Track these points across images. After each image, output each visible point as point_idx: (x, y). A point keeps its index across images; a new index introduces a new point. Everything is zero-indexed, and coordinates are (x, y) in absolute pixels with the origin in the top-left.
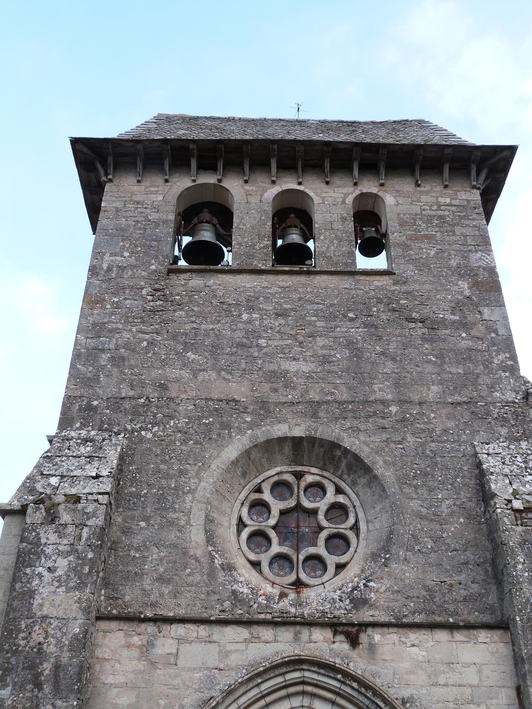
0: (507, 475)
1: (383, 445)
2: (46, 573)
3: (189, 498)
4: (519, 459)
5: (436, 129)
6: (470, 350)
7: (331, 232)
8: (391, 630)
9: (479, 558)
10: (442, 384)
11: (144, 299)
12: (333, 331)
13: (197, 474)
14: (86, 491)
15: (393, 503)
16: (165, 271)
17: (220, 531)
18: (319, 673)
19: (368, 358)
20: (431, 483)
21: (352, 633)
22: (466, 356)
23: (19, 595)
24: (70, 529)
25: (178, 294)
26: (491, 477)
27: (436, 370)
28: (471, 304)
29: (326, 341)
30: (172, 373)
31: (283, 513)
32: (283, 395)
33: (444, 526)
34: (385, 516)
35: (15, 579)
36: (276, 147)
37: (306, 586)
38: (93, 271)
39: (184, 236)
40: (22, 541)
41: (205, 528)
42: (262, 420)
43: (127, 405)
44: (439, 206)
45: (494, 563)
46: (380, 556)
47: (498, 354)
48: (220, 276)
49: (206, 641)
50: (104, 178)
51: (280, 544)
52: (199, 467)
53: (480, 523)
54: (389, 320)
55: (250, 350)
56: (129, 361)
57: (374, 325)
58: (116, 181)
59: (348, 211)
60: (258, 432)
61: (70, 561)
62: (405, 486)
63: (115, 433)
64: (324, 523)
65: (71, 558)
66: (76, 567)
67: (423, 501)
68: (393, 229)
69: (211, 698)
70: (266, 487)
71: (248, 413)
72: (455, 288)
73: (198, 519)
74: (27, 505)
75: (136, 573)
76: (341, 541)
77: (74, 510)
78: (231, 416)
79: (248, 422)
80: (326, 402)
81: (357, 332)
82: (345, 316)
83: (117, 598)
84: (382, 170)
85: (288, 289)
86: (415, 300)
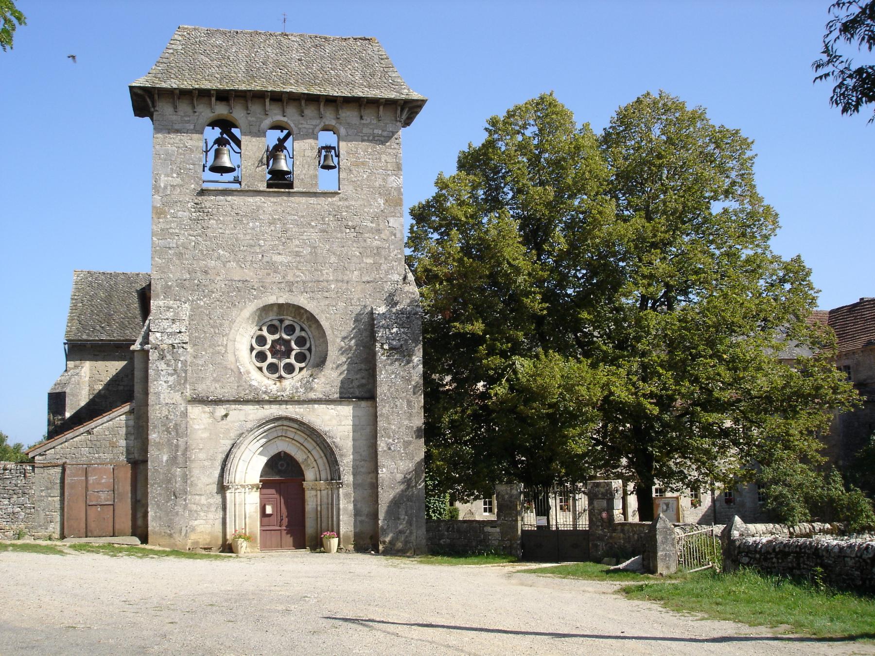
31: (273, 341)
44: (374, 137)
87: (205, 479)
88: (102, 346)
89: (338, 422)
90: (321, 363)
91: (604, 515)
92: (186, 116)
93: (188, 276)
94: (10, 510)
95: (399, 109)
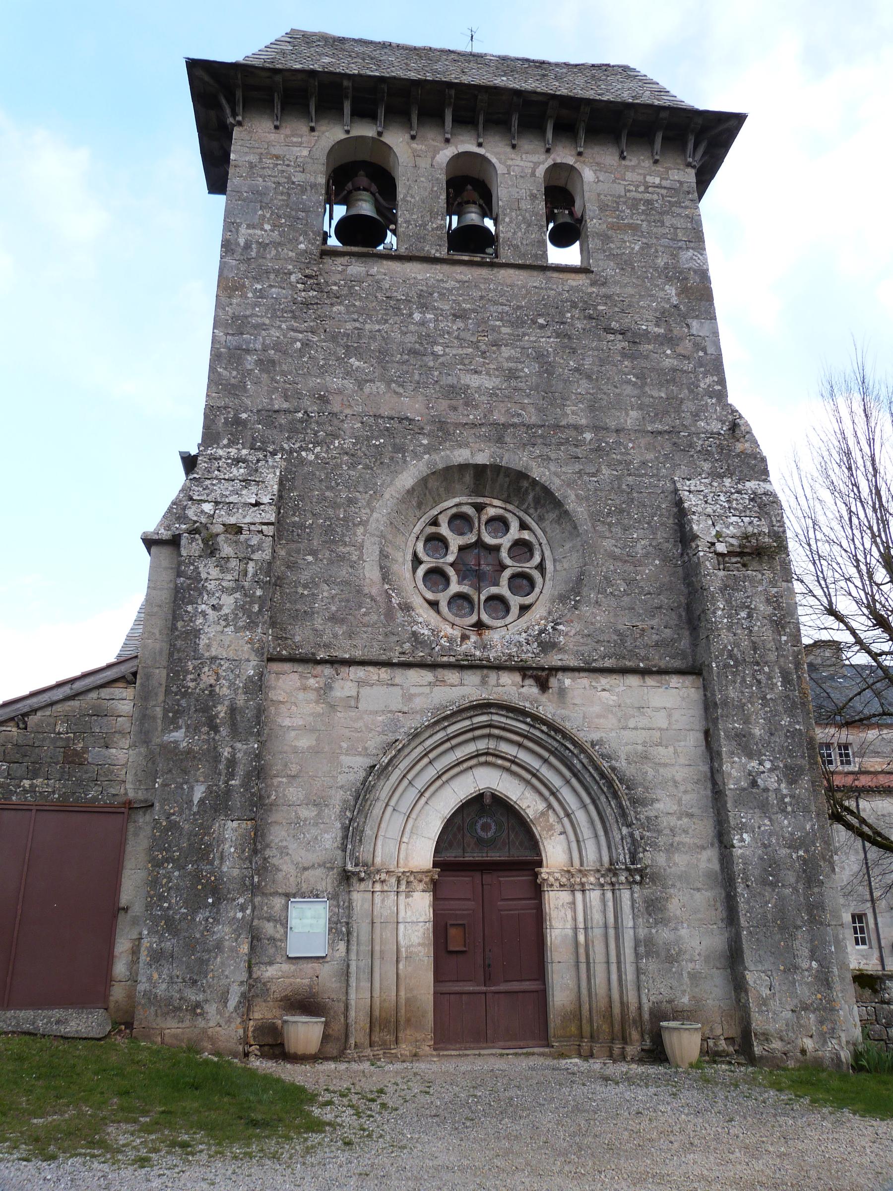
0: (709, 516)
1: (576, 477)
2: (210, 611)
3: (360, 530)
4: (722, 498)
5: (645, 81)
6: (675, 370)
7: (518, 212)
8: (582, 674)
9: (673, 602)
10: (641, 409)
11: (293, 287)
12: (520, 340)
13: (369, 504)
14: (248, 520)
15: (585, 542)
16: (316, 252)
17: (395, 568)
18: (507, 717)
19: (560, 375)
20: (626, 521)
21: (542, 677)
22: (671, 377)
23: (182, 634)
24: (233, 563)
25: (335, 284)
26: (693, 517)
27: (636, 392)
28: (679, 315)
29: (512, 351)
30: (333, 382)
31: (461, 549)
32: (463, 415)
33: (638, 568)
34: (575, 555)
35: (175, 618)
36: (453, 92)
37: (488, 627)
38: (227, 246)
39: (336, 204)
40: (179, 574)
41: (380, 565)
42: (440, 444)
43: (282, 420)
44: (647, 187)
45: (689, 608)
46: (569, 598)
47: (705, 377)
48: (385, 262)
49: (388, 684)
50: (231, 120)
51: (459, 583)
52: (371, 495)
53: (676, 566)
54: (584, 330)
55: (424, 358)
56: (280, 366)
57: (567, 334)
58: (247, 125)
59: (537, 186)
60: (436, 457)
61: (237, 599)
62: (599, 523)
63: (270, 452)
64: (508, 561)
65: (237, 595)
66: (243, 605)
67: (617, 541)
68: (591, 214)
69: (396, 741)
70: (444, 520)
71: (424, 434)
72: (662, 294)
73: (371, 553)
74: (179, 535)
75: (305, 612)
76: (525, 582)
77: (236, 542)
78: (405, 438)
79: (424, 445)
80: (512, 425)
81: (548, 343)
82: (534, 322)
83: (286, 638)
84: (582, 135)
85: (467, 284)
86: (615, 305)
87: (304, 843)
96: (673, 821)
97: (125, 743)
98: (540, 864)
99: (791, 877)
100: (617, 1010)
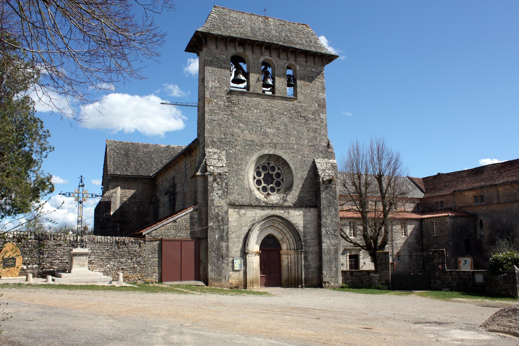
3: (243, 172)
64: (275, 178)
70: (260, 167)
88: (126, 178)
89: (297, 217)
90: (289, 188)
91: (440, 267)
92: (222, 51)
93: (224, 137)
94: (132, 266)
95: (325, 59)
96: (310, 241)
97: (197, 225)
98: (281, 249)
99: (332, 252)
100: (296, 279)
